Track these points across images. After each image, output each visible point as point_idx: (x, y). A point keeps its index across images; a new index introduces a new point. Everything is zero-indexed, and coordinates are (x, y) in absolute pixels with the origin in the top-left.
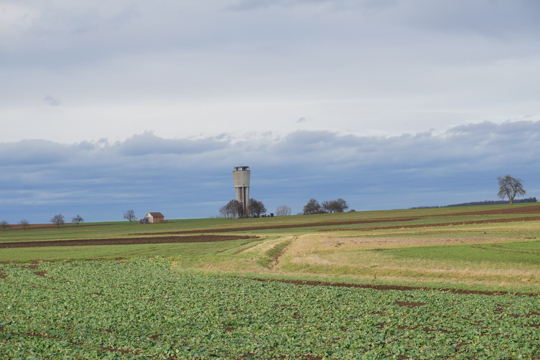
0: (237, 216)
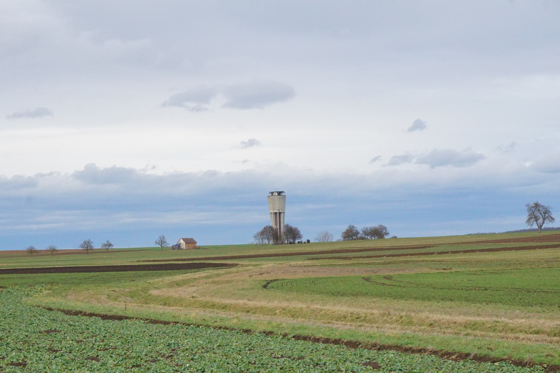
0: (271, 242)
